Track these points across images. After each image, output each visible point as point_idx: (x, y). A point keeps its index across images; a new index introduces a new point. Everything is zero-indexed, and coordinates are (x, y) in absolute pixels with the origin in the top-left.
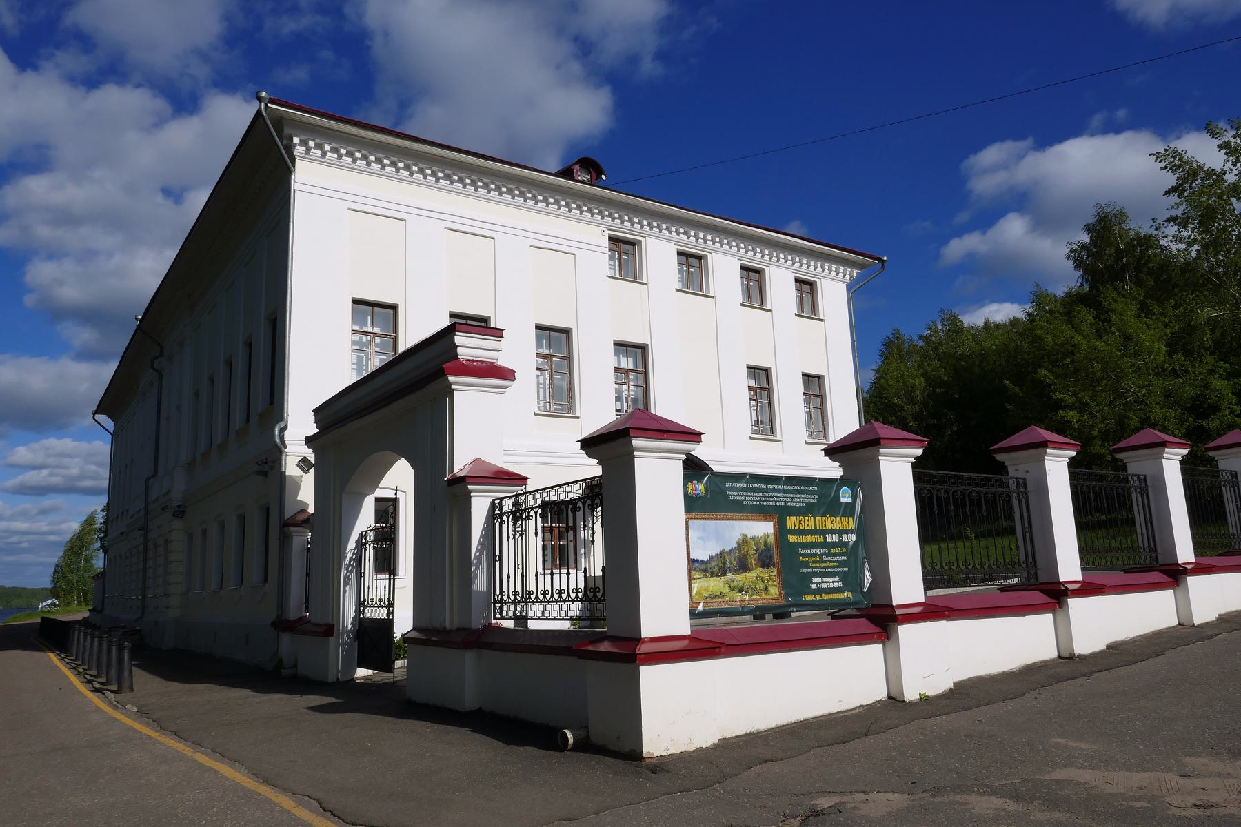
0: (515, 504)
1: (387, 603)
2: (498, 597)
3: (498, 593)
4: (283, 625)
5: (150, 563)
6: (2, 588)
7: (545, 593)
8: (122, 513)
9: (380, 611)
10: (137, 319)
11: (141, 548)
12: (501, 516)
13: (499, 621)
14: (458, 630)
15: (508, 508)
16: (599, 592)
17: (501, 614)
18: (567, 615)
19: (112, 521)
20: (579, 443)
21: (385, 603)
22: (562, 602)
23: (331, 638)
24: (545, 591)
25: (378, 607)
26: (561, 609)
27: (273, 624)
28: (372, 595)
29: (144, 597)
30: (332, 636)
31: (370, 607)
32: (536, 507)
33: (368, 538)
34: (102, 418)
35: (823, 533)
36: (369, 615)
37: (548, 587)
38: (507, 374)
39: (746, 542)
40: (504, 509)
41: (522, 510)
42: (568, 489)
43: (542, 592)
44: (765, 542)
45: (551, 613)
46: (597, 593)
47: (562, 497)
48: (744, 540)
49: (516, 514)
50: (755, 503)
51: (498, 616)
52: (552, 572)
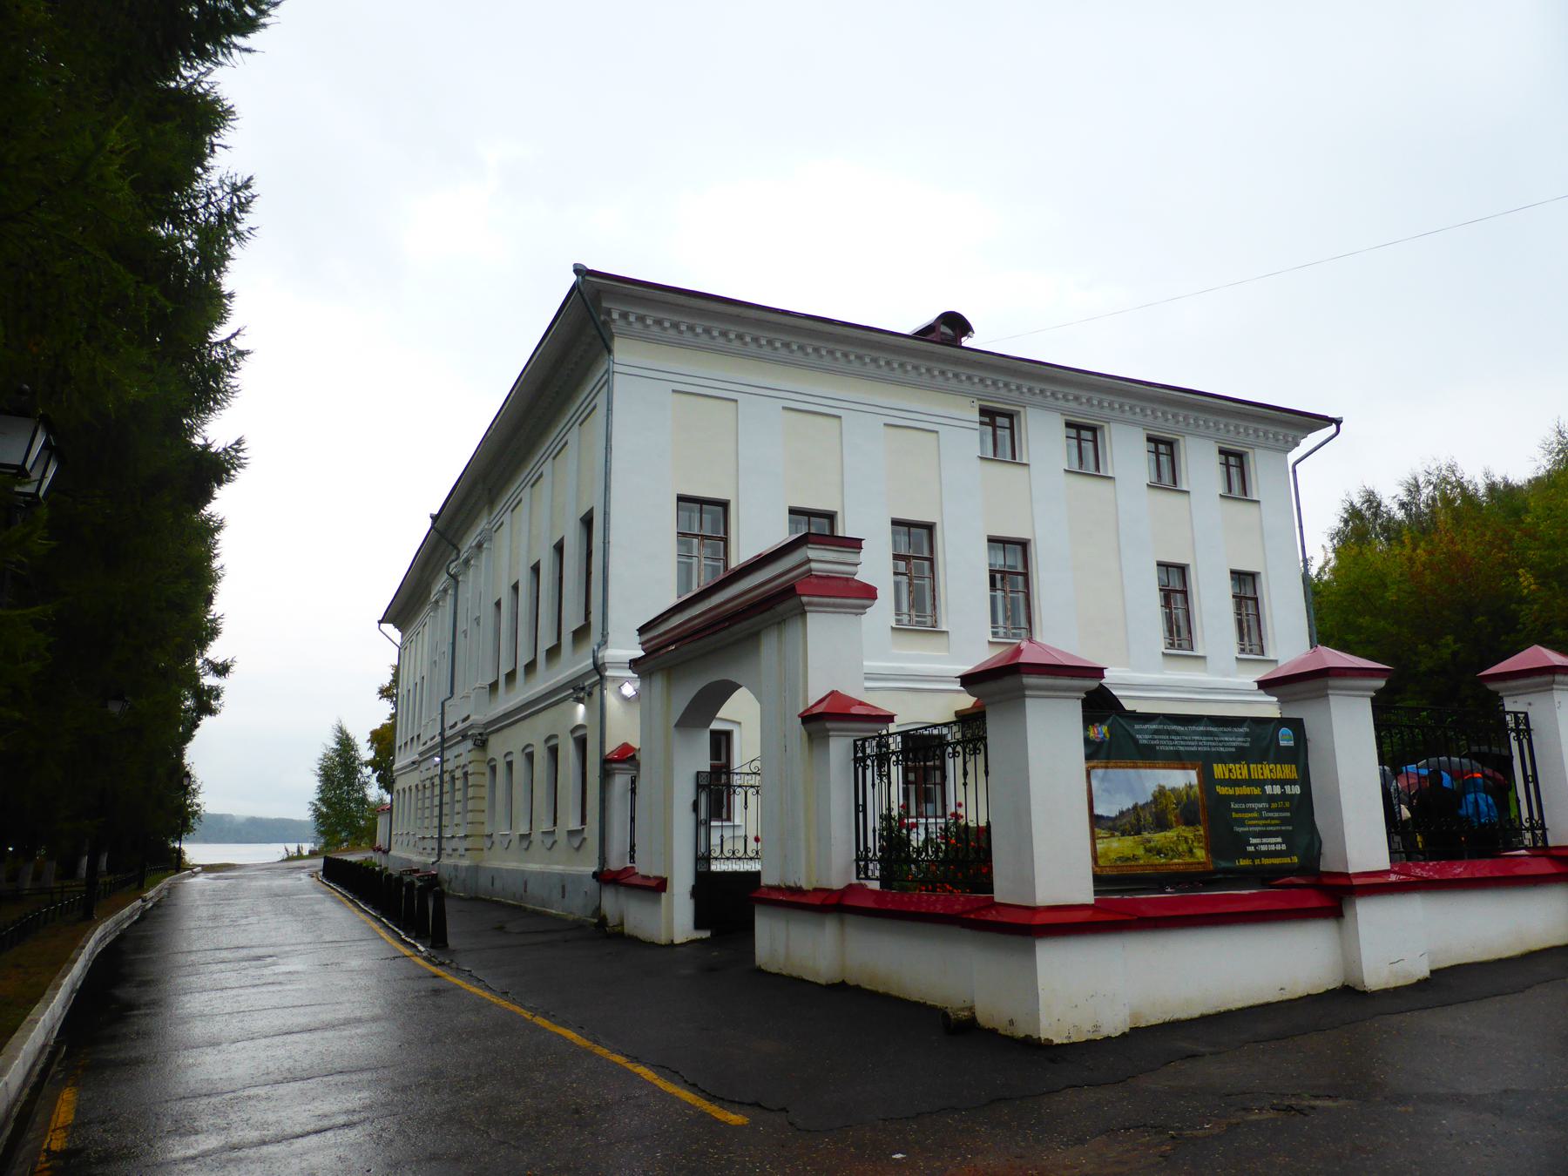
2: (862, 853)
3: (862, 848)
4: (605, 878)
5: (446, 798)
11: (437, 781)
12: (864, 759)
13: (863, 882)
14: (816, 890)
17: (866, 873)
19: (400, 747)
20: (959, 679)
23: (663, 894)
27: (595, 875)
29: (440, 838)
34: (389, 628)
35: (1261, 783)
38: (869, 593)
39: (1165, 795)
40: (868, 751)
48: (1161, 792)
50: (1172, 748)
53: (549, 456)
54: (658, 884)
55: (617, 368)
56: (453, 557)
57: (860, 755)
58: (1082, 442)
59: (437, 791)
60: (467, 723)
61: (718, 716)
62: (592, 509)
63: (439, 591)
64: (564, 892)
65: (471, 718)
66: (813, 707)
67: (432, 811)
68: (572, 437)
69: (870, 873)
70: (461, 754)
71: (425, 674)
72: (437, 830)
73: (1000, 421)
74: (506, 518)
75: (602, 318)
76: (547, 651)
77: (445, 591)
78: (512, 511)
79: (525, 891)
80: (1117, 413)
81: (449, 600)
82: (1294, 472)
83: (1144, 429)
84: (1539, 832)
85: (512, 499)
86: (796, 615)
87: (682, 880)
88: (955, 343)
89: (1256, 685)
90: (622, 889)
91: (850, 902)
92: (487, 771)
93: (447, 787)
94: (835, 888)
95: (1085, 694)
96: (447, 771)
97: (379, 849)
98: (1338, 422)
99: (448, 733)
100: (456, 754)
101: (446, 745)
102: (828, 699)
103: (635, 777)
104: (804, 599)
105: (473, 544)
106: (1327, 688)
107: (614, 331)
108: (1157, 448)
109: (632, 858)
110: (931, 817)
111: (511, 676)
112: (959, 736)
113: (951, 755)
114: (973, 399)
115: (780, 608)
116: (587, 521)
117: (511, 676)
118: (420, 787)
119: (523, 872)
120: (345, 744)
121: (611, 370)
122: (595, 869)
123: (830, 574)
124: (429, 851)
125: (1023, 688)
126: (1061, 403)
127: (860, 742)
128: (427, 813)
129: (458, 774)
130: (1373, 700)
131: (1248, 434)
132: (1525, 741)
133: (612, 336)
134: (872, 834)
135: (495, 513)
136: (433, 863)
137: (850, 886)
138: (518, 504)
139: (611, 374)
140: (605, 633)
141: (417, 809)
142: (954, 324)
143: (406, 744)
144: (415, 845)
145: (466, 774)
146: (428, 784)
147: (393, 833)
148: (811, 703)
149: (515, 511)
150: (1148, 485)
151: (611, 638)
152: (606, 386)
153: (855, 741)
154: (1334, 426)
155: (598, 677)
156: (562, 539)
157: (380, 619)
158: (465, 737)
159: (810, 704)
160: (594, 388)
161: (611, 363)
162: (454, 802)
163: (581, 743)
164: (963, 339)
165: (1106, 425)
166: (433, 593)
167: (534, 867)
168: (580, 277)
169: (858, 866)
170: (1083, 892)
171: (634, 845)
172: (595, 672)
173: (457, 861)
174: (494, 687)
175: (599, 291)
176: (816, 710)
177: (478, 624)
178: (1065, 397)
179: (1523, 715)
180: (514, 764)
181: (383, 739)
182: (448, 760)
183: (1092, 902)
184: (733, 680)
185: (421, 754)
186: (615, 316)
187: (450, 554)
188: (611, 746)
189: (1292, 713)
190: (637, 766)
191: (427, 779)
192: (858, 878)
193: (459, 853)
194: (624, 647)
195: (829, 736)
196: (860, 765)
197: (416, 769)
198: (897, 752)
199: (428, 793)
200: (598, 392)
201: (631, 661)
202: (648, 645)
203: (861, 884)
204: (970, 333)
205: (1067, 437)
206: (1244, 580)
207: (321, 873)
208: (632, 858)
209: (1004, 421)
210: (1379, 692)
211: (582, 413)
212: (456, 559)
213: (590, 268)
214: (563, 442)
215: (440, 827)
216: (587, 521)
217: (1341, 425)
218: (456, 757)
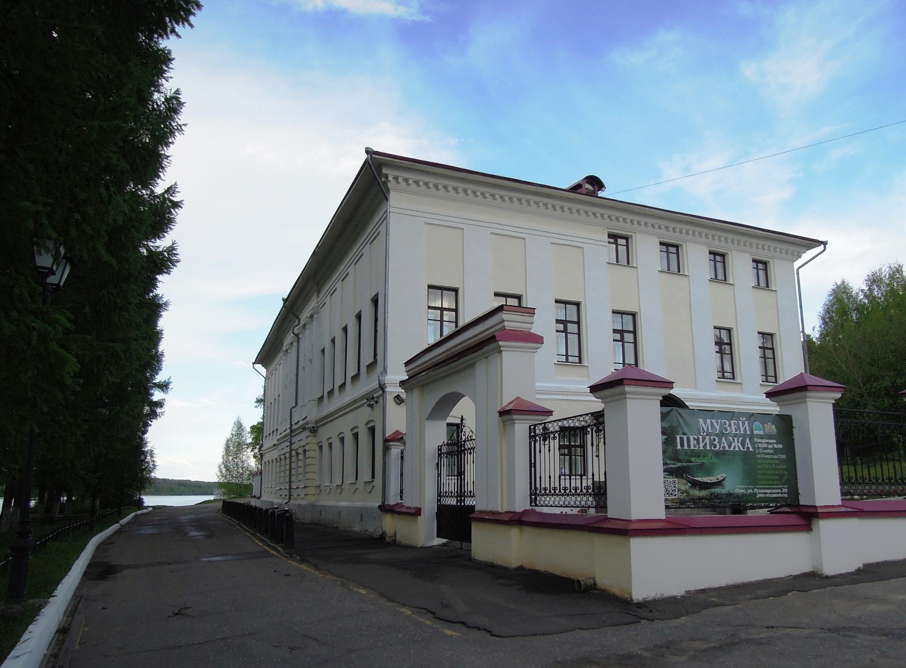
0: (545, 428)
1: (456, 494)
2: (533, 491)
3: (533, 488)
4: (385, 508)
5: (293, 465)
7: (576, 489)
8: (273, 431)
9: (471, 500)
11: (288, 455)
12: (535, 437)
13: (534, 508)
14: (507, 512)
15: (540, 431)
18: (580, 504)
19: (266, 437)
20: (589, 388)
21: (454, 494)
22: (588, 495)
23: (419, 517)
24: (576, 488)
25: (450, 497)
26: (576, 500)
27: (380, 507)
28: (545, 484)
29: (290, 488)
30: (420, 515)
31: (469, 497)
32: (592, 425)
33: (466, 447)
34: (259, 367)
36: (444, 502)
37: (447, 490)
38: (538, 340)
40: (537, 432)
41: (549, 433)
42: (581, 419)
43: (586, 488)
45: (549, 502)
47: (577, 424)
49: (545, 436)
51: (533, 504)
53: (328, 294)
54: (416, 512)
55: (391, 210)
56: (296, 323)
57: (533, 434)
58: (717, 262)
59: (288, 461)
60: (305, 421)
62: (378, 293)
63: (307, 317)
64: (362, 517)
65: (307, 418)
67: (285, 473)
68: (366, 251)
69: (538, 503)
70: (302, 439)
71: (280, 393)
72: (288, 484)
73: (621, 241)
74: (328, 300)
75: (383, 180)
76: (352, 377)
77: (292, 343)
78: (331, 295)
79: (339, 518)
80: (690, 237)
81: (294, 349)
82: (798, 273)
83: (707, 246)
85: (330, 289)
86: (496, 353)
87: (429, 507)
88: (593, 194)
90: (396, 515)
91: (525, 519)
92: (317, 448)
93: (294, 459)
94: (517, 511)
95: (662, 397)
96: (294, 449)
97: (255, 497)
98: (825, 243)
99: (294, 427)
100: (299, 439)
101: (293, 434)
102: (513, 403)
103: (403, 450)
105: (308, 316)
106: (806, 397)
107: (389, 187)
108: (757, 266)
110: (573, 475)
111: (331, 392)
114: (604, 228)
115: (486, 349)
116: (375, 301)
117: (331, 392)
118: (278, 460)
119: (338, 507)
120: (239, 426)
121: (388, 211)
122: (380, 504)
123: (516, 329)
124: (283, 496)
125: (625, 393)
126: (657, 230)
127: (533, 427)
128: (282, 475)
129: (301, 451)
130: (834, 405)
131: (721, 241)
133: (388, 191)
134: (539, 480)
135: (320, 298)
136: (286, 503)
137: (526, 511)
139: (388, 213)
140: (386, 366)
141: (277, 472)
142: (595, 182)
143: (273, 431)
144: (275, 494)
145: (305, 451)
146: (283, 457)
147: (263, 487)
148: (505, 404)
149: (332, 296)
150: (709, 280)
151: (388, 369)
152: (385, 221)
153: (530, 426)
154: (822, 246)
155: (382, 392)
156: (360, 312)
157: (254, 361)
158: (304, 429)
159: (504, 406)
160: (375, 226)
161: (388, 207)
162: (298, 460)
163: (372, 431)
164: (599, 192)
165: (684, 244)
166: (285, 345)
167: (344, 504)
168: (369, 155)
169: (531, 498)
170: (660, 513)
171: (402, 490)
172: (380, 389)
173: (300, 502)
174: (321, 399)
175: (381, 163)
176: (507, 408)
177: (311, 363)
178: (660, 228)
180: (333, 445)
181: (258, 430)
182: (294, 443)
184: (460, 392)
185: (278, 440)
186: (390, 178)
187: (295, 321)
188: (389, 433)
189: (786, 412)
190: (404, 444)
191: (282, 455)
192: (531, 506)
193: (300, 497)
194: (396, 374)
195: (514, 423)
197: (276, 449)
199: (283, 463)
200: (382, 223)
201: (400, 382)
203: (533, 509)
204: (603, 189)
205: (710, 260)
206: (767, 336)
207: (221, 510)
208: (401, 497)
209: (623, 242)
211: (374, 234)
212: (298, 325)
213: (375, 150)
214: (361, 253)
215: (290, 482)
216: (375, 301)
217: (827, 246)
218: (299, 441)
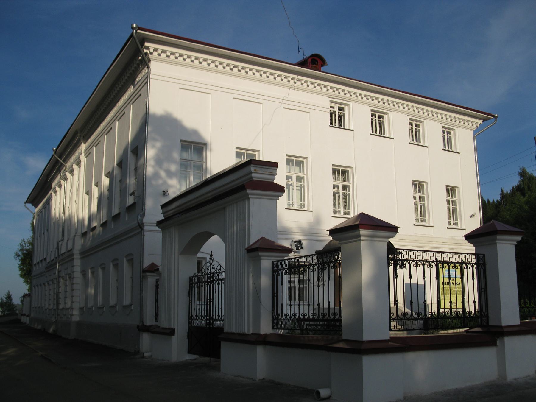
2: (275, 316)
6: (535, 318)
10: (53, 150)
14: (252, 334)
16: (306, 316)
17: (277, 326)
20: (328, 232)
23: (173, 336)
36: (194, 324)
44: (59, 220)
46: (287, 317)
52: (299, 303)
61: (200, 251)
66: (253, 244)
84: (484, 319)
89: (464, 238)
95: (517, 242)
104: (249, 191)
109: (156, 320)
112: (316, 261)
113: (312, 270)
127: (276, 263)
132: (482, 270)
138: (99, 143)
153: (273, 262)
179: (482, 256)
183: (518, 323)
188: (146, 263)
196: (275, 273)
198: (286, 269)
202: (166, 214)
210: (519, 243)
214: (123, 112)
